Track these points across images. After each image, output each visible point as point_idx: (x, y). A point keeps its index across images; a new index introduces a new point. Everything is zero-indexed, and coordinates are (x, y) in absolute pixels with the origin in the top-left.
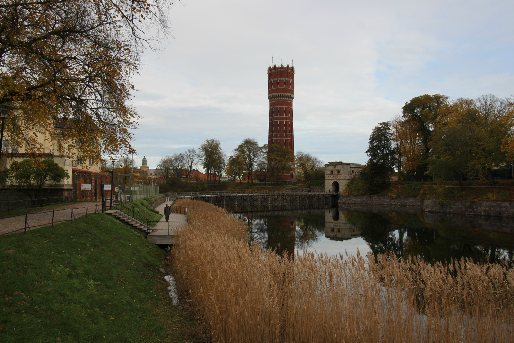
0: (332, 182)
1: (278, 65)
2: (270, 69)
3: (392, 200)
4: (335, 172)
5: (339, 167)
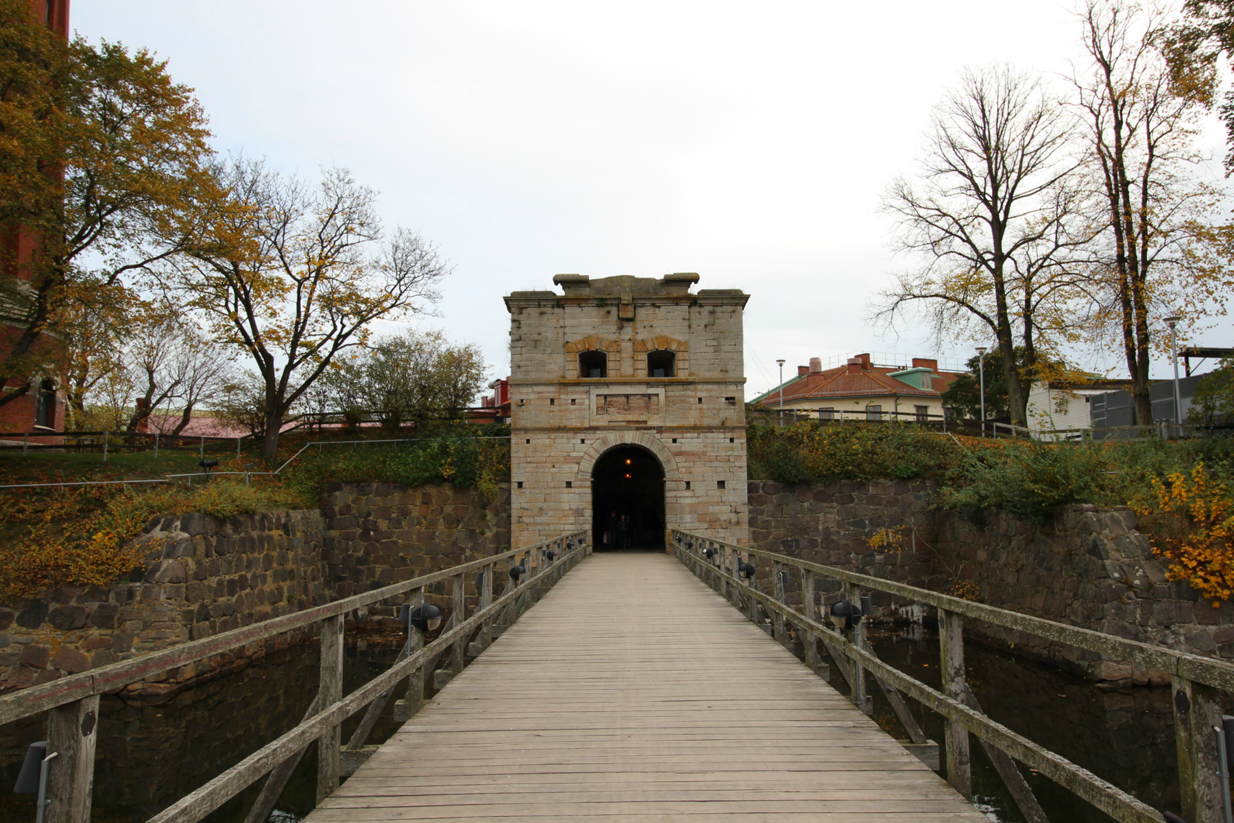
0: (590, 450)
4: (627, 365)
5: (664, 326)
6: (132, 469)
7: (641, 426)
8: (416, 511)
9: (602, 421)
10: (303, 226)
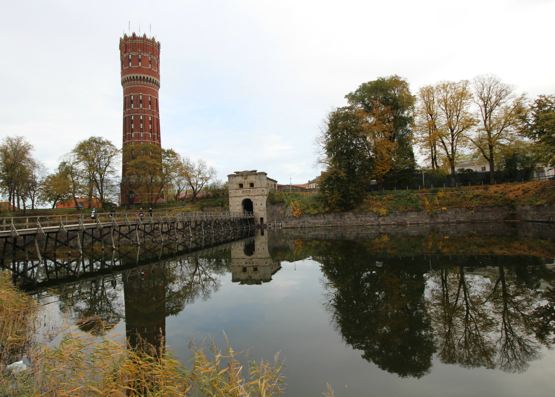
0: (241, 200)
1: (139, 34)
3: (381, 219)
4: (247, 186)
5: (252, 179)
6: (175, 206)
7: (249, 195)
8: (216, 210)
9: (243, 195)
10: (196, 168)
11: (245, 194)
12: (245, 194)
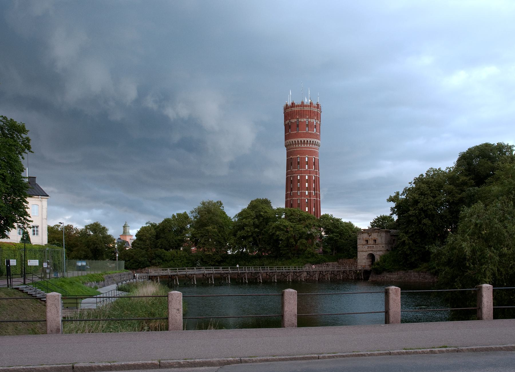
2: (286, 107)
4: (371, 242)
11: (370, 249)
12: (370, 249)
